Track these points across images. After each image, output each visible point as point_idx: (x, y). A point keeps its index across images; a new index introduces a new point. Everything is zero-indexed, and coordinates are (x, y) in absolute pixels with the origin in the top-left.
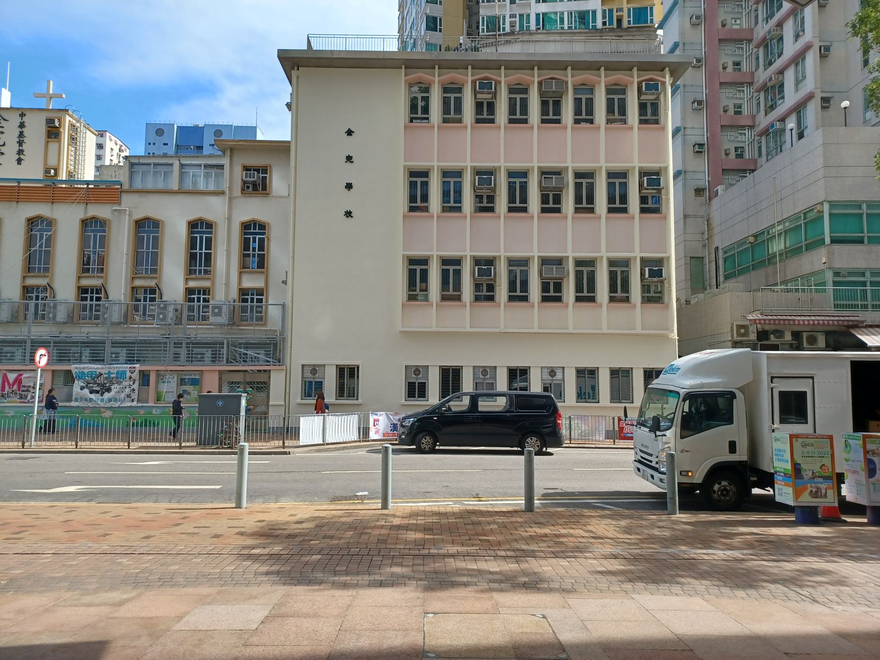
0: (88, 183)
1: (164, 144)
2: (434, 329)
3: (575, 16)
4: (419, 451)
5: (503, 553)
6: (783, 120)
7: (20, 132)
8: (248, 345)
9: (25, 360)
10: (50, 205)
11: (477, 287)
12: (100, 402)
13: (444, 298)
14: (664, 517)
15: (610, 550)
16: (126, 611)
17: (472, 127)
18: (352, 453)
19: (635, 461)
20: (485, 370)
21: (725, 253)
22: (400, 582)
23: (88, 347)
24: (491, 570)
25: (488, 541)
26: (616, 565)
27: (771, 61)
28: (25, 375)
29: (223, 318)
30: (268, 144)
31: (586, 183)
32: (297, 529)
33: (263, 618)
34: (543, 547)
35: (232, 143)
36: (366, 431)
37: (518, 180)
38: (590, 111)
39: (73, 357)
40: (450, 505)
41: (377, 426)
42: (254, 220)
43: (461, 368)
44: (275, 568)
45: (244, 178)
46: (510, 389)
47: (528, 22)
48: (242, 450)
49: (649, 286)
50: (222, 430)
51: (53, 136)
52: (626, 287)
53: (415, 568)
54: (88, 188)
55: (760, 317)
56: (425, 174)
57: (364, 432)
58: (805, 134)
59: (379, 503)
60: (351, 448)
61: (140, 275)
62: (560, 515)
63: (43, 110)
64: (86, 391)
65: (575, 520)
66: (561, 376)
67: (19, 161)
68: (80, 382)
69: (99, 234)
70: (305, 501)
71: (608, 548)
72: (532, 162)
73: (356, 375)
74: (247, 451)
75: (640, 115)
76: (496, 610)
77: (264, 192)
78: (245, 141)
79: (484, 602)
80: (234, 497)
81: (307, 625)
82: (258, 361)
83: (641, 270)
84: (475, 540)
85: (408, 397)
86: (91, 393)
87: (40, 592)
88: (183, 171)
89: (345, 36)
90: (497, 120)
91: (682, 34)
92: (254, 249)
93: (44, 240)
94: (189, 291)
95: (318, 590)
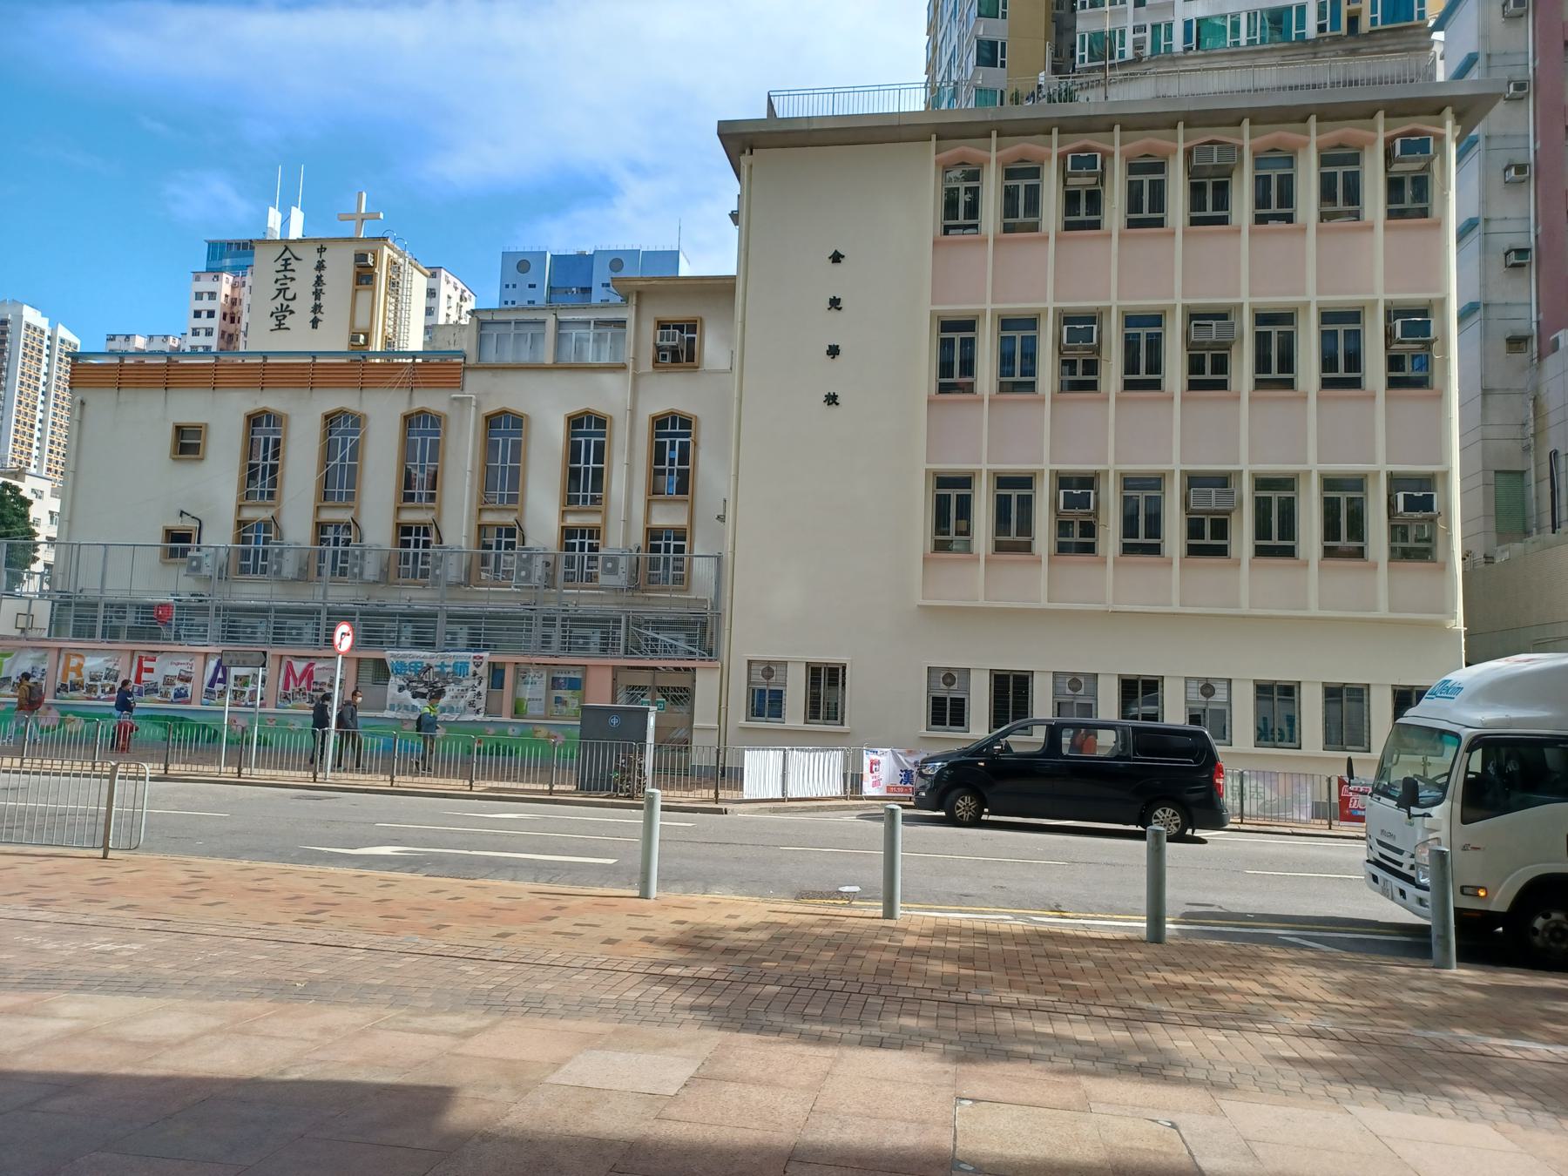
0: (414, 355)
1: (530, 286)
2: (981, 603)
3: (1262, 18)
4: (952, 821)
5: (1103, 1012)
8: (659, 625)
9: (318, 640)
10: (357, 392)
11: (1063, 527)
13: (1000, 548)
14: (1425, 972)
15: (1309, 1022)
16: (471, 1047)
17: (1057, 238)
18: (832, 818)
19: (1368, 861)
20: (1075, 681)
22: (915, 1043)
23: (409, 621)
24: (1079, 1037)
25: (1076, 988)
26: (1319, 1050)
28: (318, 665)
30: (699, 282)
31: (1279, 332)
32: (739, 939)
33: (686, 1079)
34: (1179, 1007)
35: (640, 283)
36: (857, 782)
38: (1287, 198)
39: (389, 637)
40: (1006, 921)
41: (876, 774)
43: (1030, 674)
44: (704, 1000)
45: (658, 341)
46: (1124, 717)
47: (1169, 37)
48: (651, 802)
49: (1405, 528)
50: (617, 767)
51: (364, 281)
53: (942, 1022)
54: (414, 363)
56: (969, 325)
57: (854, 782)
59: (878, 907)
60: (831, 809)
61: (491, 506)
62: (1217, 954)
63: (350, 239)
64: (407, 694)
65: (1240, 964)
66: (1226, 697)
69: (429, 438)
70: (752, 895)
71: (1304, 1018)
72: (1173, 297)
73: (840, 681)
74: (658, 804)
75: (1390, 200)
76: (1085, 1105)
77: (690, 364)
78: (661, 279)
79: (1064, 1090)
80: (637, 878)
81: (759, 1098)
82: (676, 652)
83: (1389, 496)
84: (1052, 984)
86: (414, 697)
87: (352, 1005)
88: (561, 332)
89: (832, 91)
90: (1105, 224)
91: (1484, 36)
92: (672, 462)
93: (348, 449)
94: (568, 532)
95: (775, 1042)
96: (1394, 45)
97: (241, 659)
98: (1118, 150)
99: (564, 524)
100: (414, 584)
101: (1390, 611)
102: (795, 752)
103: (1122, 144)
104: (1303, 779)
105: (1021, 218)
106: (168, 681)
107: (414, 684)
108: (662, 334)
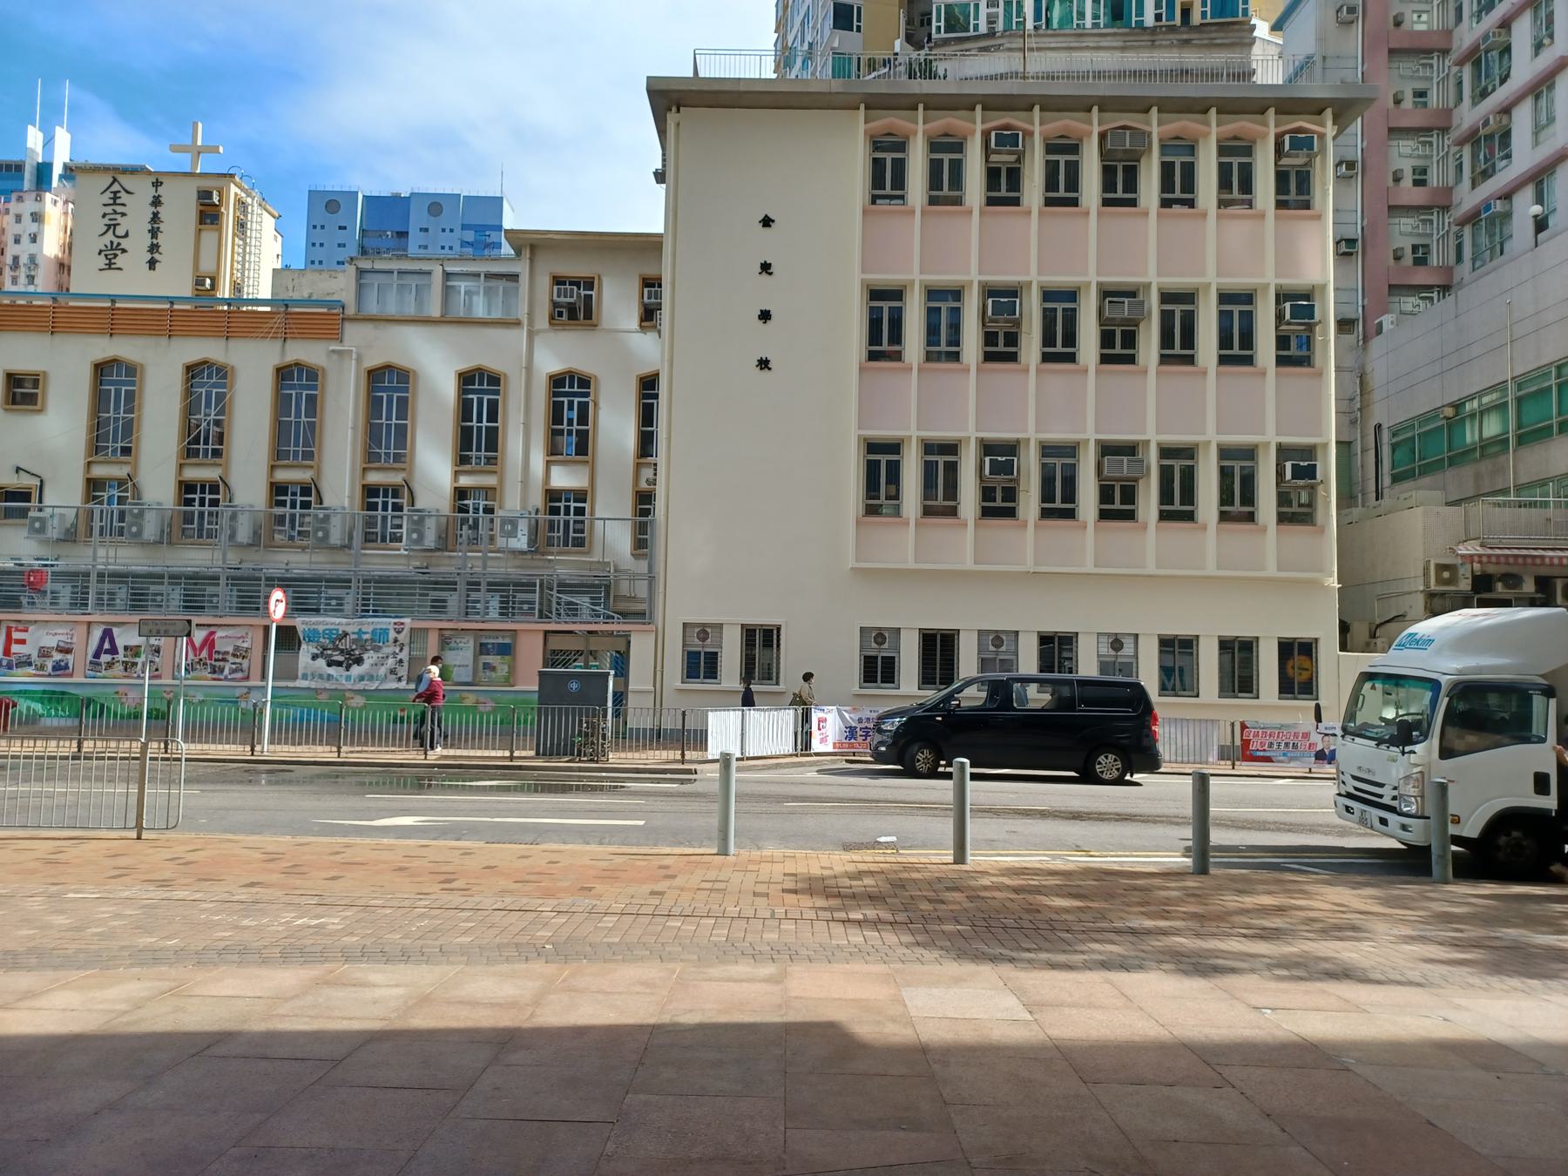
1: (340, 228)
4: (911, 772)
6: (1507, 196)
7: (153, 213)
8: (564, 587)
12: (344, 682)
13: (928, 512)
20: (998, 638)
21: (1394, 435)
27: (1485, 89)
28: (220, 633)
29: (519, 540)
30: (597, 238)
37: (1060, 306)
38: (1189, 184)
42: (570, 372)
45: (555, 298)
50: (580, 731)
51: (208, 221)
52: (1249, 497)
55: (1481, 551)
56: (897, 294)
58: (1551, 222)
59: (949, 855)
63: (185, 174)
64: (321, 662)
66: (1133, 650)
67: (152, 264)
68: (310, 647)
73: (775, 641)
77: (588, 322)
85: (865, 681)
86: (329, 665)
88: (449, 283)
91: (1321, 39)
92: (570, 422)
96: (1222, 38)
97: (163, 629)
98: (1038, 128)
99: (457, 485)
100: (292, 547)
101: (1157, 568)
102: (752, 712)
103: (1041, 124)
104: (1209, 724)
105: (946, 191)
106: (44, 653)
107: (329, 652)
108: (650, 292)
